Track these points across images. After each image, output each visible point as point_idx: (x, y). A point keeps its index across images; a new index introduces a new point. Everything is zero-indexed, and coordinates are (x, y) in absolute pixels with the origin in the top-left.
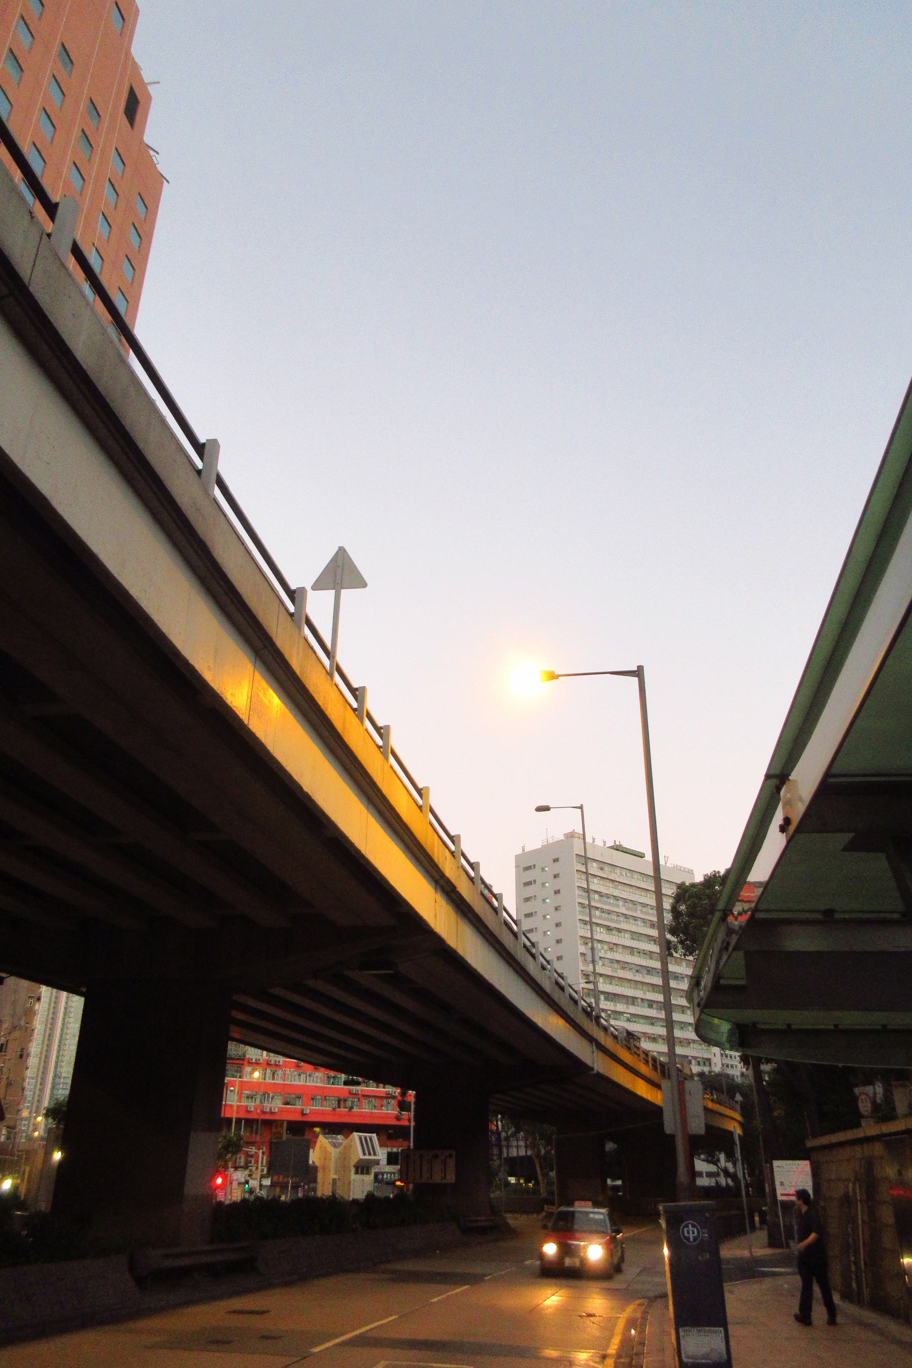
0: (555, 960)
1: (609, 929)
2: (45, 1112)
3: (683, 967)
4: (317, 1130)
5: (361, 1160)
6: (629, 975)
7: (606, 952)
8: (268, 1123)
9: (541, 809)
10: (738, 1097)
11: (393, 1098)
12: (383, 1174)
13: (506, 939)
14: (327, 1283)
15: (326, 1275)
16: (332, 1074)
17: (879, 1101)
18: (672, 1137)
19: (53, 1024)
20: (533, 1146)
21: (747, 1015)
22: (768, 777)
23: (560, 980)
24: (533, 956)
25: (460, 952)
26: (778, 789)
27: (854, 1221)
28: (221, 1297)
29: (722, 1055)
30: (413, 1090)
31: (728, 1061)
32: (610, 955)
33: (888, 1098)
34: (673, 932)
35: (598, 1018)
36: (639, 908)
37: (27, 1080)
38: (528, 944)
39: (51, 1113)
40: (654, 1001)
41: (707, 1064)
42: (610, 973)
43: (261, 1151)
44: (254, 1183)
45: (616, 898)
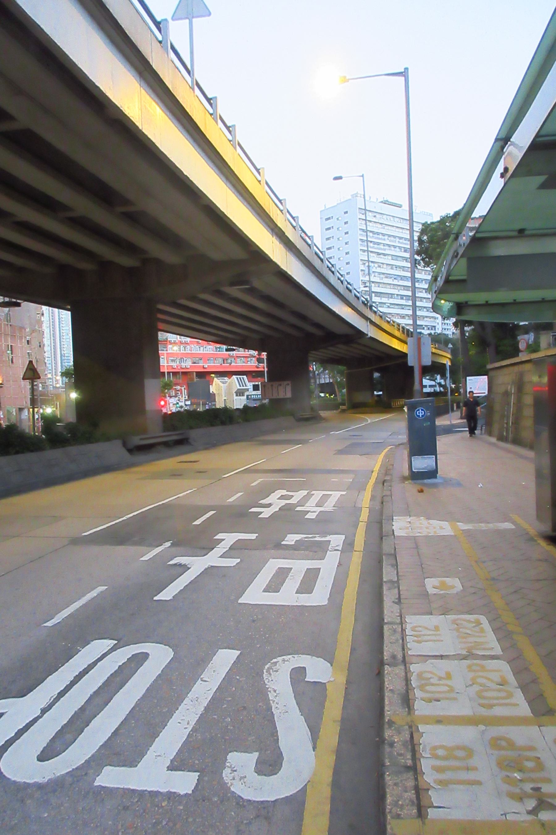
0: (346, 274)
1: (379, 254)
2: (60, 374)
3: (424, 274)
4: (213, 375)
5: (238, 389)
6: (390, 281)
7: (376, 268)
8: (185, 373)
9: (336, 178)
10: (450, 346)
11: (255, 357)
12: (251, 395)
13: (317, 263)
14: (225, 447)
15: (224, 444)
16: (218, 346)
17: (530, 343)
18: (412, 368)
19: (54, 328)
20: (333, 377)
21: (461, 297)
22: (497, 140)
23: (349, 286)
24: (333, 272)
25: (289, 273)
26: (503, 148)
27: (509, 404)
28: (175, 456)
29: (442, 323)
30: (265, 352)
31: (446, 327)
32: (379, 270)
33: (537, 342)
34: (418, 253)
35: (371, 307)
36: (398, 240)
37: (47, 359)
38: (330, 266)
39: (65, 374)
40: (404, 296)
41: (433, 329)
42: (379, 281)
43: (183, 388)
44: (182, 404)
45: (383, 235)
